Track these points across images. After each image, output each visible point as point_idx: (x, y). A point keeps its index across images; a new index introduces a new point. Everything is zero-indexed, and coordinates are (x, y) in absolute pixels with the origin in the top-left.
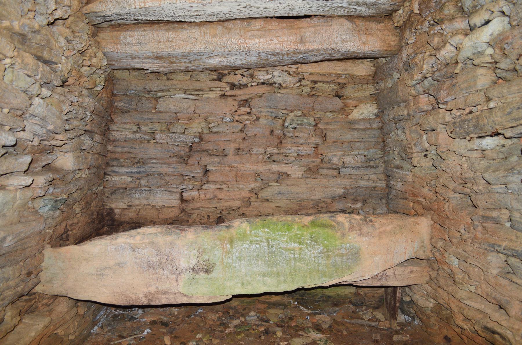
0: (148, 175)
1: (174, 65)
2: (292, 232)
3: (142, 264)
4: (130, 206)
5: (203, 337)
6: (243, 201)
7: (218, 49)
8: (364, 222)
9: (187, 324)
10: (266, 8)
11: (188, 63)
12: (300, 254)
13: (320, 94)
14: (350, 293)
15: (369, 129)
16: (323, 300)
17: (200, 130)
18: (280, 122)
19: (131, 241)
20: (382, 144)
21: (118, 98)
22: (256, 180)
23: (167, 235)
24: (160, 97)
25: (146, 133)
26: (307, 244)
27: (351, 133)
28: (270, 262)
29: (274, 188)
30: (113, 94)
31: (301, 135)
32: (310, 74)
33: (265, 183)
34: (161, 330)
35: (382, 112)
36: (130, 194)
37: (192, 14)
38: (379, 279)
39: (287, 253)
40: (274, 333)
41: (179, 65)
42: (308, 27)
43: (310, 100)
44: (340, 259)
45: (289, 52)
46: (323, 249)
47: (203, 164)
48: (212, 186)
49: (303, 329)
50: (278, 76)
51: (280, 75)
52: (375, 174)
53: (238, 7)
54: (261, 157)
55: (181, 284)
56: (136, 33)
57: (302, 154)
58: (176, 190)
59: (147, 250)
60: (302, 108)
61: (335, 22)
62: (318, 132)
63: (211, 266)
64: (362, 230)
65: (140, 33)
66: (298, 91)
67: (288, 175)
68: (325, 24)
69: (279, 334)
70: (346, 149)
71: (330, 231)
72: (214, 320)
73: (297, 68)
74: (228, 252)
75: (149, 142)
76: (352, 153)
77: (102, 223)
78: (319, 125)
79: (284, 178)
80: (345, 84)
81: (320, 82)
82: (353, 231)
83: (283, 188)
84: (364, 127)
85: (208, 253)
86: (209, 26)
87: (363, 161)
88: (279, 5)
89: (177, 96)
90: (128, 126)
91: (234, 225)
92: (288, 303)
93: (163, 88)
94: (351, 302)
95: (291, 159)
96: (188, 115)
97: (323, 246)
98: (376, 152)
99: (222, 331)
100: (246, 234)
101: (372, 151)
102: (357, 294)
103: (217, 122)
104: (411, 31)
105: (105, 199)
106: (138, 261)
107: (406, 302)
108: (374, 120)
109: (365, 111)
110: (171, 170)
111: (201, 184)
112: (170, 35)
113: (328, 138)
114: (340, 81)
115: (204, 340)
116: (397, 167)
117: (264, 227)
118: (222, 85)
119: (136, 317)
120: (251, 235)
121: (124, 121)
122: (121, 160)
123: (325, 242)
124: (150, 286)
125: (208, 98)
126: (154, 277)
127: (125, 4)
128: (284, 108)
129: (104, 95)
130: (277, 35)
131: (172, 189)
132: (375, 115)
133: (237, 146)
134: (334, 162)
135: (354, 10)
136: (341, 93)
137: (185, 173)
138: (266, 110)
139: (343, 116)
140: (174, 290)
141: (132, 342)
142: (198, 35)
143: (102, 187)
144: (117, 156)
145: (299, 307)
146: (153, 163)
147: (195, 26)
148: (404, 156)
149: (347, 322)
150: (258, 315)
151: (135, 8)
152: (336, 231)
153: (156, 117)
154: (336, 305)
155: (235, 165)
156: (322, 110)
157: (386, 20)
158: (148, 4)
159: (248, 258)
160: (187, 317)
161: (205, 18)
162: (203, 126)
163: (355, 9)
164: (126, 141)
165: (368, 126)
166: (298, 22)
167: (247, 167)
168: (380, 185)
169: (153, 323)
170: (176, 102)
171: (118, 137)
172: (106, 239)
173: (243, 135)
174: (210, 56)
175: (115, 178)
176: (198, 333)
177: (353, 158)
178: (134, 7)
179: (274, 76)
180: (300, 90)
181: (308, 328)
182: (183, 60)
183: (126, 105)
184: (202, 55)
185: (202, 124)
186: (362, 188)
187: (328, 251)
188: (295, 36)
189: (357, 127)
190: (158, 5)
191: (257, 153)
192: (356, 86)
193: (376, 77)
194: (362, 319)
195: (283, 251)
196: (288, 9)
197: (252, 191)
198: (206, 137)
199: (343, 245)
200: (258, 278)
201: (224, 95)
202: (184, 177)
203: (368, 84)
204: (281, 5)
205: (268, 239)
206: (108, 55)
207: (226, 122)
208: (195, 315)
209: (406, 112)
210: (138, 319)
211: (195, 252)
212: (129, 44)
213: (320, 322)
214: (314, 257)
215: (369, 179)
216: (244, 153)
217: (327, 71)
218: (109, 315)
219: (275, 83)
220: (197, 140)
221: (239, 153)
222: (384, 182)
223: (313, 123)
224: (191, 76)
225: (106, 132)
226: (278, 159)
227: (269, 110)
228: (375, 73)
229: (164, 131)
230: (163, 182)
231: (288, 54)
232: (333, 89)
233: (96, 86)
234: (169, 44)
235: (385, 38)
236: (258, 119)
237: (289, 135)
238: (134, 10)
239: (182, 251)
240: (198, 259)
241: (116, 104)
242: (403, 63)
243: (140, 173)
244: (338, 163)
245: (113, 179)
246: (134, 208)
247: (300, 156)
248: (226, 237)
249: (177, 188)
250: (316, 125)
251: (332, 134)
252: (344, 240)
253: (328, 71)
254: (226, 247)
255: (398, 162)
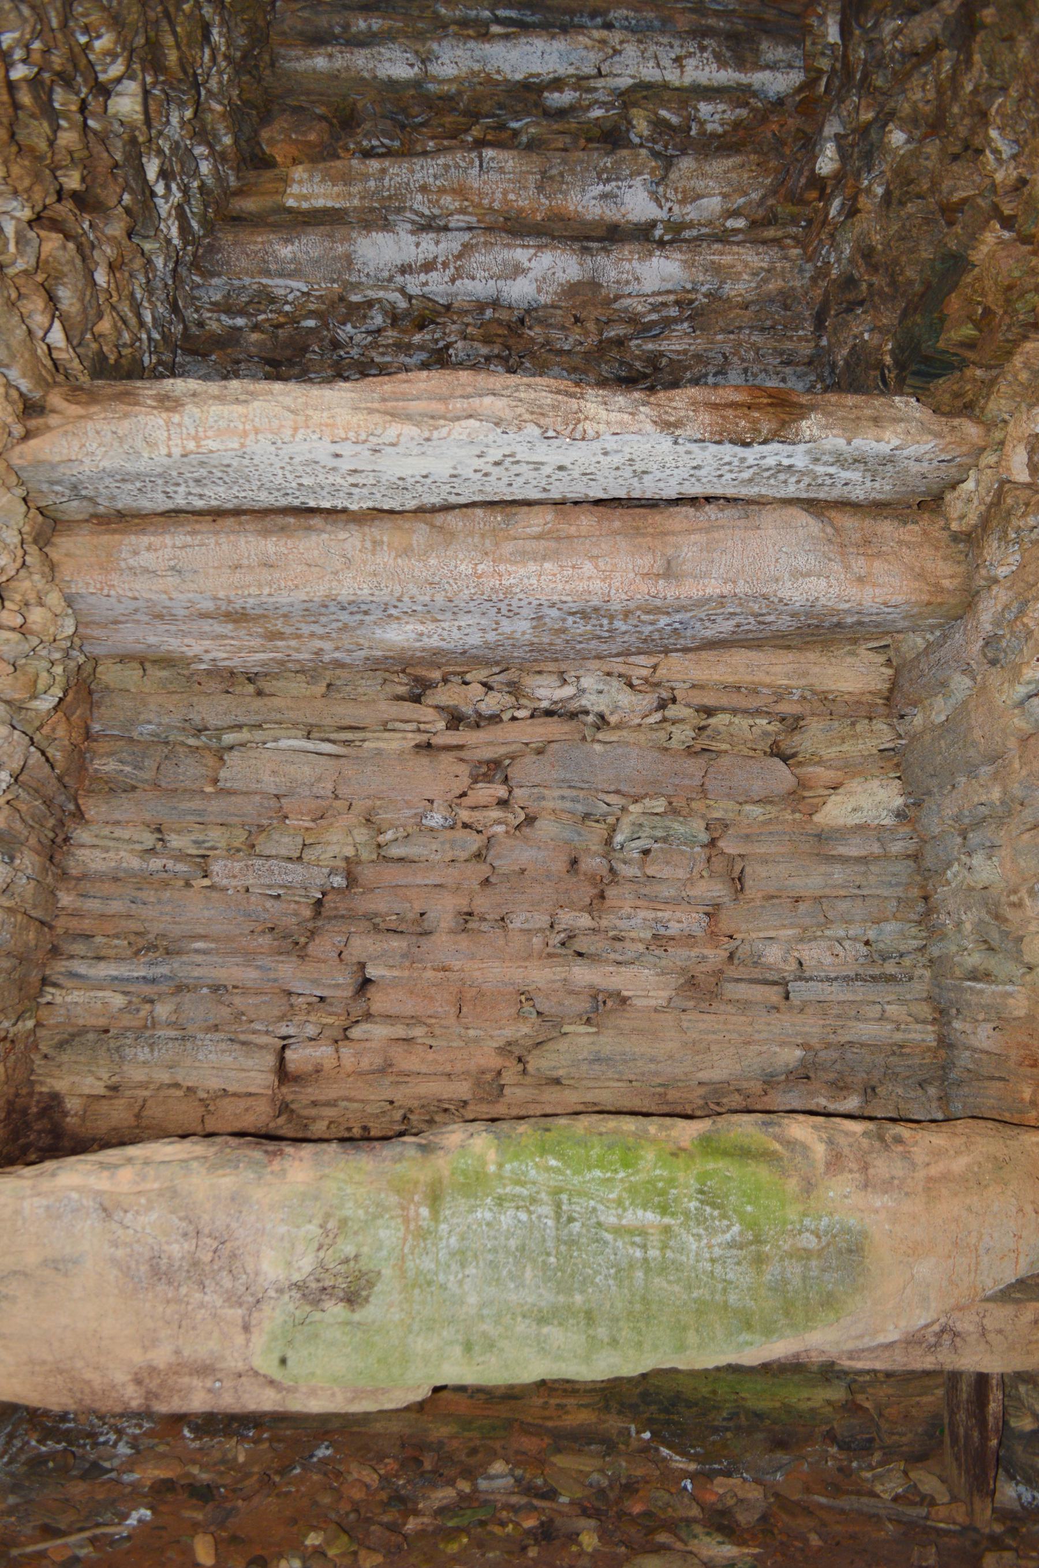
0: (180, 989)
1: (280, 643)
2: (637, 1172)
3: (133, 1264)
4: (114, 1088)
5: (329, 1542)
6: (478, 1083)
7: (414, 591)
8: (877, 1144)
9: (278, 1495)
10: (561, 468)
11: (321, 638)
12: (664, 1247)
13: (724, 747)
14: (829, 1402)
15: (877, 858)
16: (739, 1428)
17: (349, 851)
18: (600, 830)
19: (101, 1182)
20: (921, 907)
21: (102, 747)
22: (520, 1015)
23: (222, 1167)
24: (231, 748)
25: (181, 856)
26: (686, 1213)
27: (823, 868)
28: (564, 1272)
29: (581, 1040)
30: (88, 736)
31: (666, 872)
32: (694, 686)
33: (552, 1024)
34: (187, 1514)
35: (918, 804)
36: (118, 1049)
37: (339, 480)
38: (930, 1347)
39: (620, 1244)
40: (573, 1537)
41: (293, 643)
42: (689, 532)
43: (694, 766)
44: (798, 1269)
45: (632, 605)
46: (741, 1233)
47: (355, 960)
48: (379, 1031)
49: (671, 1526)
50: (595, 690)
51: (601, 687)
52: (901, 1001)
53: (478, 463)
54: (537, 941)
55: (259, 1340)
56: (168, 540)
57: (669, 932)
58: (264, 1040)
59: (154, 1216)
60: (670, 790)
61: (769, 518)
62: (718, 864)
63: (363, 1282)
64: (871, 1171)
65: (181, 539)
66: (654, 735)
67: (624, 1000)
68: (742, 523)
69: (589, 1541)
70: (807, 921)
71: (763, 1172)
72: (367, 1486)
73: (655, 667)
74: (423, 1234)
75: (188, 885)
76: (827, 933)
77: (21, 1141)
78: (721, 844)
79: (611, 1011)
80: (799, 718)
81: (724, 710)
82: (842, 1172)
83: (608, 1043)
84: (863, 853)
85: (356, 1233)
86: (387, 524)
87: (862, 960)
88: (601, 458)
89: (284, 743)
90: (126, 834)
91: (445, 1143)
92: (620, 1433)
93: (242, 719)
94: (831, 1437)
95: (634, 949)
96: (314, 804)
97: (742, 1221)
98: (902, 932)
99: (393, 1528)
100: (486, 1174)
101: (890, 927)
102: (852, 1407)
103: (404, 826)
104: (1003, 537)
105: (38, 1061)
106: (120, 1253)
107: (1022, 1436)
108: (892, 830)
109: (865, 802)
110: (250, 975)
111: (347, 1024)
112: (271, 546)
113: (748, 883)
114: (784, 708)
115: (332, 1552)
116: (974, 976)
117: (543, 1151)
118: (424, 712)
119: (107, 1465)
120: (500, 1177)
121: (117, 816)
122: (98, 939)
123: (749, 1208)
124: (155, 1342)
125: (379, 752)
126: (169, 1311)
127: (139, 444)
128: (612, 788)
129: (61, 732)
130: (595, 552)
131: (252, 1037)
132: (898, 816)
133: (462, 903)
134: (771, 960)
135: (829, 482)
136: (788, 744)
137: (297, 987)
138: (557, 793)
139: (797, 815)
140: (234, 1362)
141: (82, 1553)
142: (354, 547)
143: (30, 1024)
144: (87, 925)
145: (657, 1450)
146: (197, 951)
147: (347, 522)
148: (995, 936)
149: (821, 1507)
150: (519, 1472)
151: (169, 455)
152: (784, 1173)
153: (215, 806)
154: (780, 1444)
155: (456, 964)
156: (729, 796)
157: (926, 516)
158: (209, 442)
159: (490, 1257)
160: (277, 1472)
161: (378, 496)
162: (359, 839)
163: (831, 476)
164: (116, 879)
165: (876, 849)
166: (656, 518)
167: (493, 970)
168: (918, 1037)
169: (164, 1488)
170: (279, 761)
171: (93, 866)
172: (20, 1177)
173: (484, 870)
174: (390, 616)
175: (76, 996)
176: (314, 1528)
177: (830, 948)
178: (164, 451)
179: (584, 691)
180: (662, 735)
181: (689, 1521)
182: (306, 629)
183: (128, 769)
184: (366, 613)
185: (355, 832)
186: (862, 1045)
187: (758, 1240)
188: (650, 557)
189: (842, 850)
190: (236, 446)
191: (526, 926)
192: (836, 724)
193: (893, 701)
194: (874, 1495)
195: (609, 1237)
196: (628, 472)
197: (505, 1050)
198: (367, 874)
199: (807, 1222)
200: (522, 1327)
201: (429, 745)
202: (293, 1000)
203: (871, 719)
204: (609, 458)
205: (557, 1192)
206: (80, 605)
207: (432, 829)
208: (304, 1467)
209: (996, 794)
210: (113, 1475)
211: (313, 1229)
212: (146, 570)
213: (731, 1502)
214: (713, 1261)
215: (882, 1018)
216: (484, 926)
217: (744, 677)
218: (17, 1454)
219: (587, 713)
220: (338, 881)
221: (470, 925)
222: (930, 1028)
223: (704, 837)
224: (329, 685)
225: (55, 849)
226: (592, 950)
227: (567, 792)
228: (894, 685)
229: (238, 850)
230: (225, 1012)
231: (627, 614)
232: (766, 734)
233: (34, 697)
234: (265, 575)
235: (922, 568)
236: (530, 820)
237: (627, 871)
238: (166, 461)
239: (269, 1226)
240: (321, 1254)
241: (97, 764)
242: (981, 643)
243: (153, 981)
244: (782, 965)
245: (69, 999)
246: (128, 1093)
247: (660, 941)
248: (416, 1183)
249: (267, 1032)
250: (713, 843)
251: (762, 871)
252: (813, 1203)
253: (749, 678)
254: (418, 1214)
255: (974, 959)
